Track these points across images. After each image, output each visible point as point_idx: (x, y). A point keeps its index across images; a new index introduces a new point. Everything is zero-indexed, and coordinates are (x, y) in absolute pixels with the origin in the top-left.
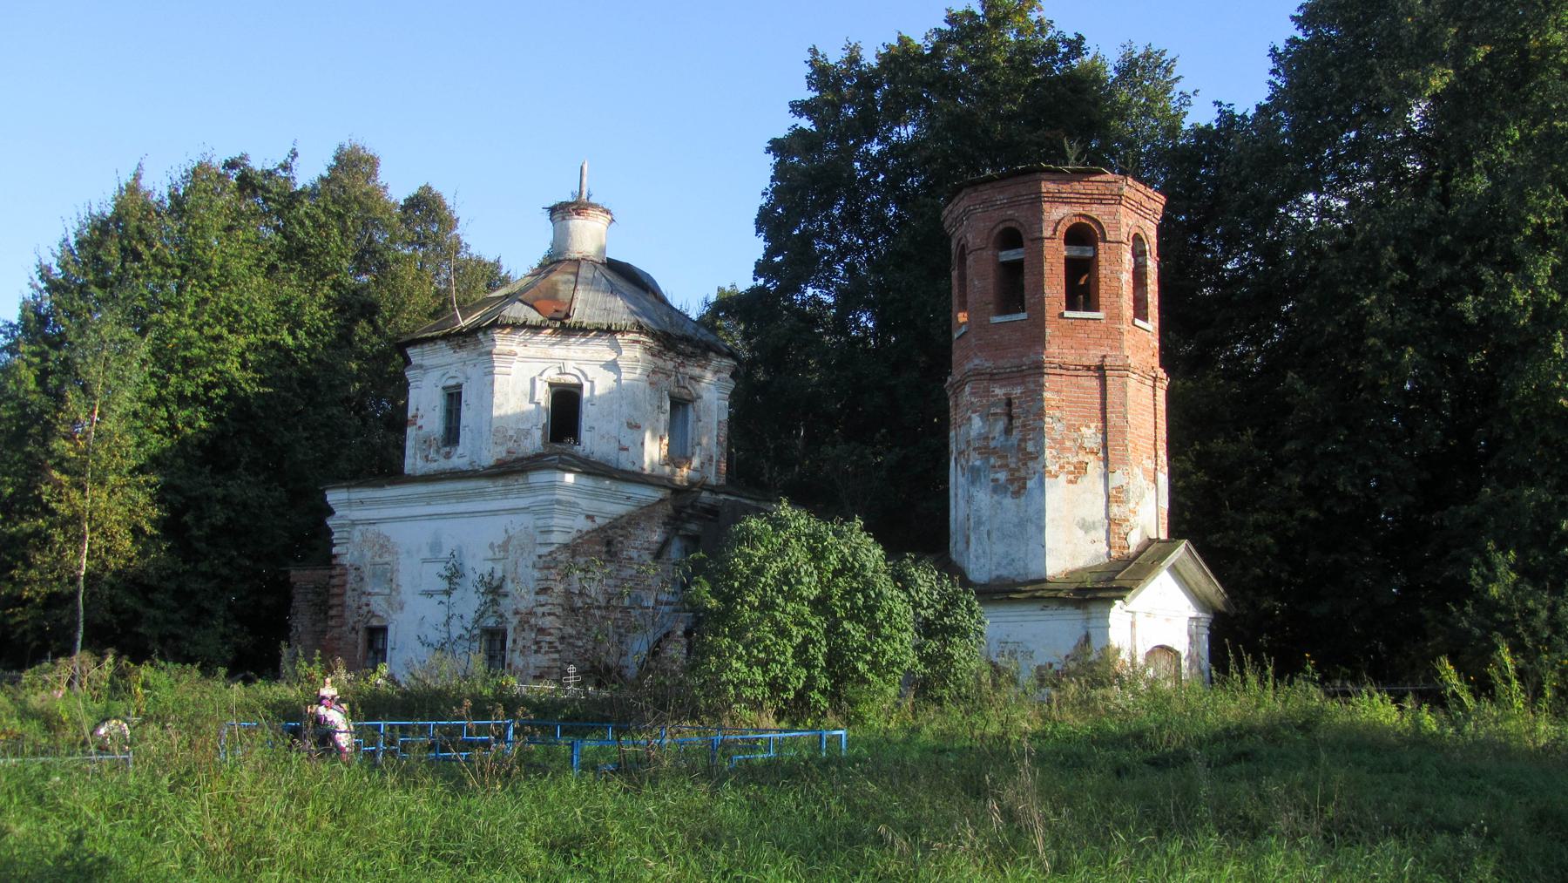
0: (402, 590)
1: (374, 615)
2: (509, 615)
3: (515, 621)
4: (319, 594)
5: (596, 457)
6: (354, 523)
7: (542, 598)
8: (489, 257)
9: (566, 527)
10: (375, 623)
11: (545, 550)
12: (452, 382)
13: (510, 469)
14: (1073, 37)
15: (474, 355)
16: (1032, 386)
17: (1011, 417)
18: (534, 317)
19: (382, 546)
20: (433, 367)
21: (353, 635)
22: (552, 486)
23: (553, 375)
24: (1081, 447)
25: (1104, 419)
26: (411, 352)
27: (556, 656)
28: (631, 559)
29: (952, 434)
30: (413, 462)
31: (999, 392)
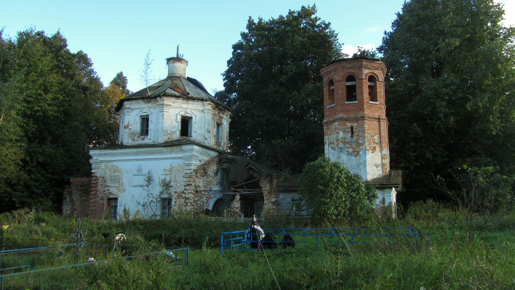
1: (111, 194)
2: (173, 193)
3: (176, 195)
6: (101, 162)
7: (188, 188)
9: (195, 164)
10: (111, 196)
12: (145, 114)
13: (170, 144)
14: (327, 23)
15: (155, 105)
16: (361, 123)
17: (352, 133)
18: (178, 94)
19: (114, 170)
20: (136, 109)
22: (192, 150)
23: (183, 113)
25: (380, 134)
27: (192, 207)
31: (349, 125)
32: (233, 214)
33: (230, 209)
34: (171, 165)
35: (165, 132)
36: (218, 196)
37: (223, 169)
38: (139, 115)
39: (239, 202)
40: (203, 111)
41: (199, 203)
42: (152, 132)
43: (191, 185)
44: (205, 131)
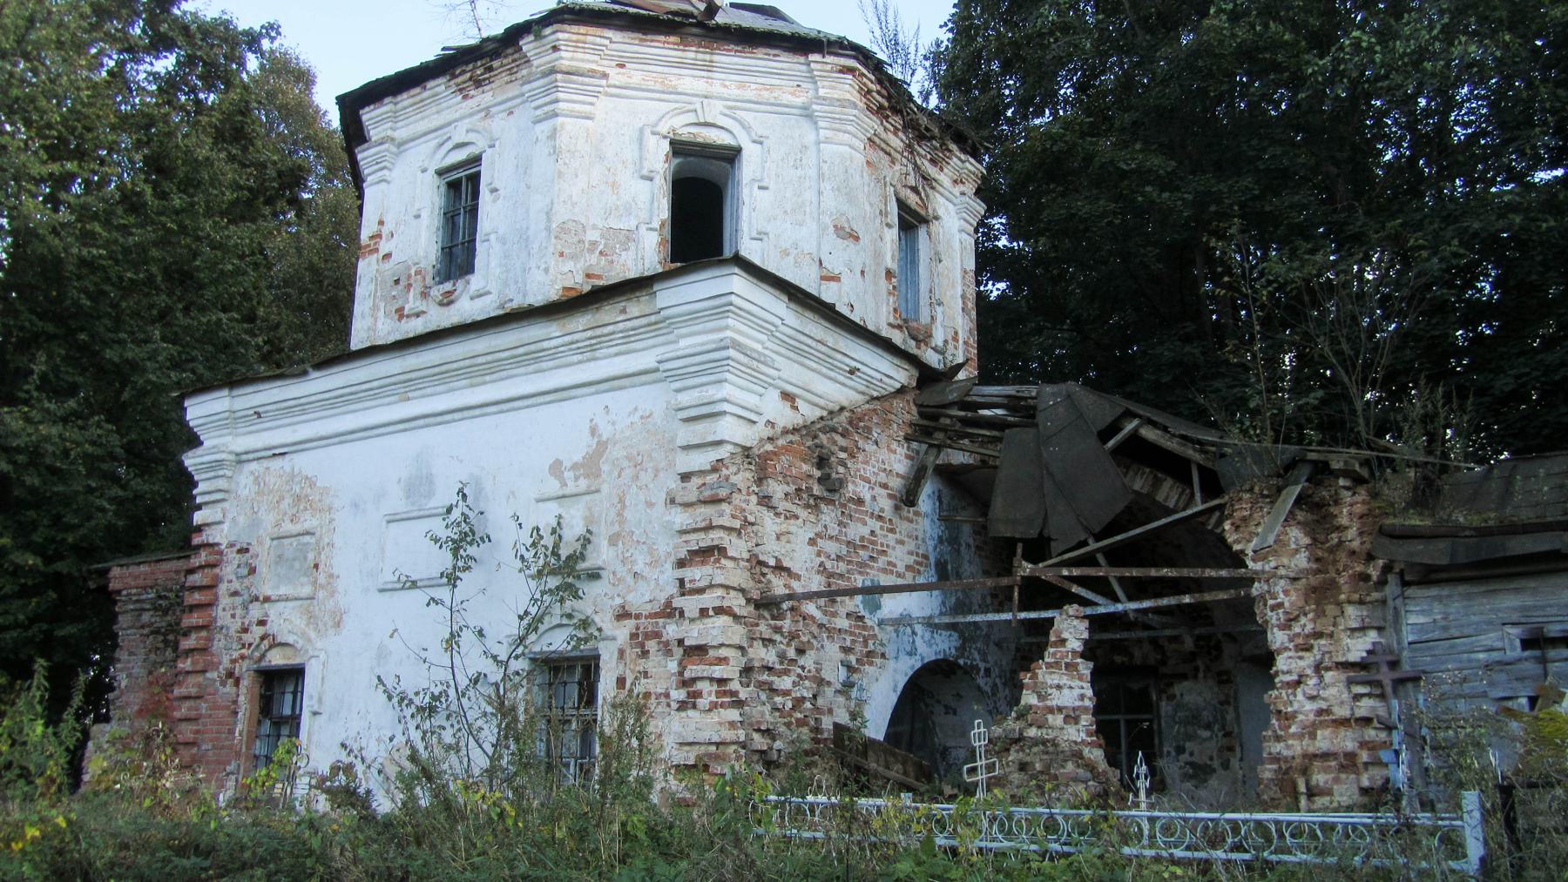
0: (341, 585)
2: (604, 621)
3: (622, 632)
6: (241, 459)
7: (697, 574)
9: (752, 408)
10: (276, 659)
11: (701, 460)
12: (461, 156)
21: (229, 688)
27: (734, 714)
28: (860, 502)
30: (370, 321)
32: (1042, 770)
33: (1012, 724)
35: (567, 234)
36: (934, 646)
37: (949, 475)
39: (1085, 668)
40: (807, 113)
41: (785, 683)
42: (496, 248)
43: (722, 551)
44: (823, 229)
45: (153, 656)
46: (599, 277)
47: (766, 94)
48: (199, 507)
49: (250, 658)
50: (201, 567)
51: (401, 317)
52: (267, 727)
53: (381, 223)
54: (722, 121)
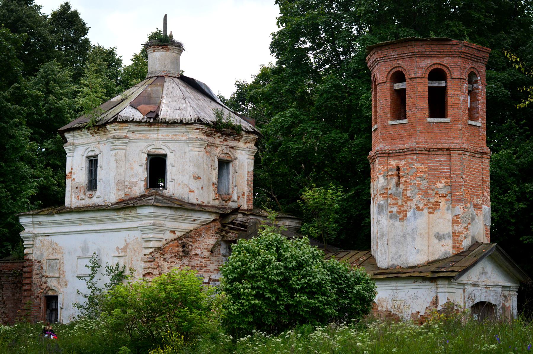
0: (66, 274)
4: (16, 277)
5: (176, 196)
6: (36, 236)
7: (147, 278)
8: (107, 46)
10: (50, 293)
11: (148, 251)
12: (92, 154)
13: (126, 205)
16: (410, 160)
18: (138, 116)
19: (53, 249)
24: (437, 194)
26: (66, 135)
28: (197, 254)
29: (371, 184)
31: (393, 163)
34: (125, 240)
38: (85, 155)
44: (190, 177)
45: (13, 290)
46: (128, 195)
47: (174, 137)
48: (25, 248)
49: (43, 292)
50: (27, 266)
51: (79, 199)
52: (49, 311)
53: (72, 169)
54: (162, 147)
